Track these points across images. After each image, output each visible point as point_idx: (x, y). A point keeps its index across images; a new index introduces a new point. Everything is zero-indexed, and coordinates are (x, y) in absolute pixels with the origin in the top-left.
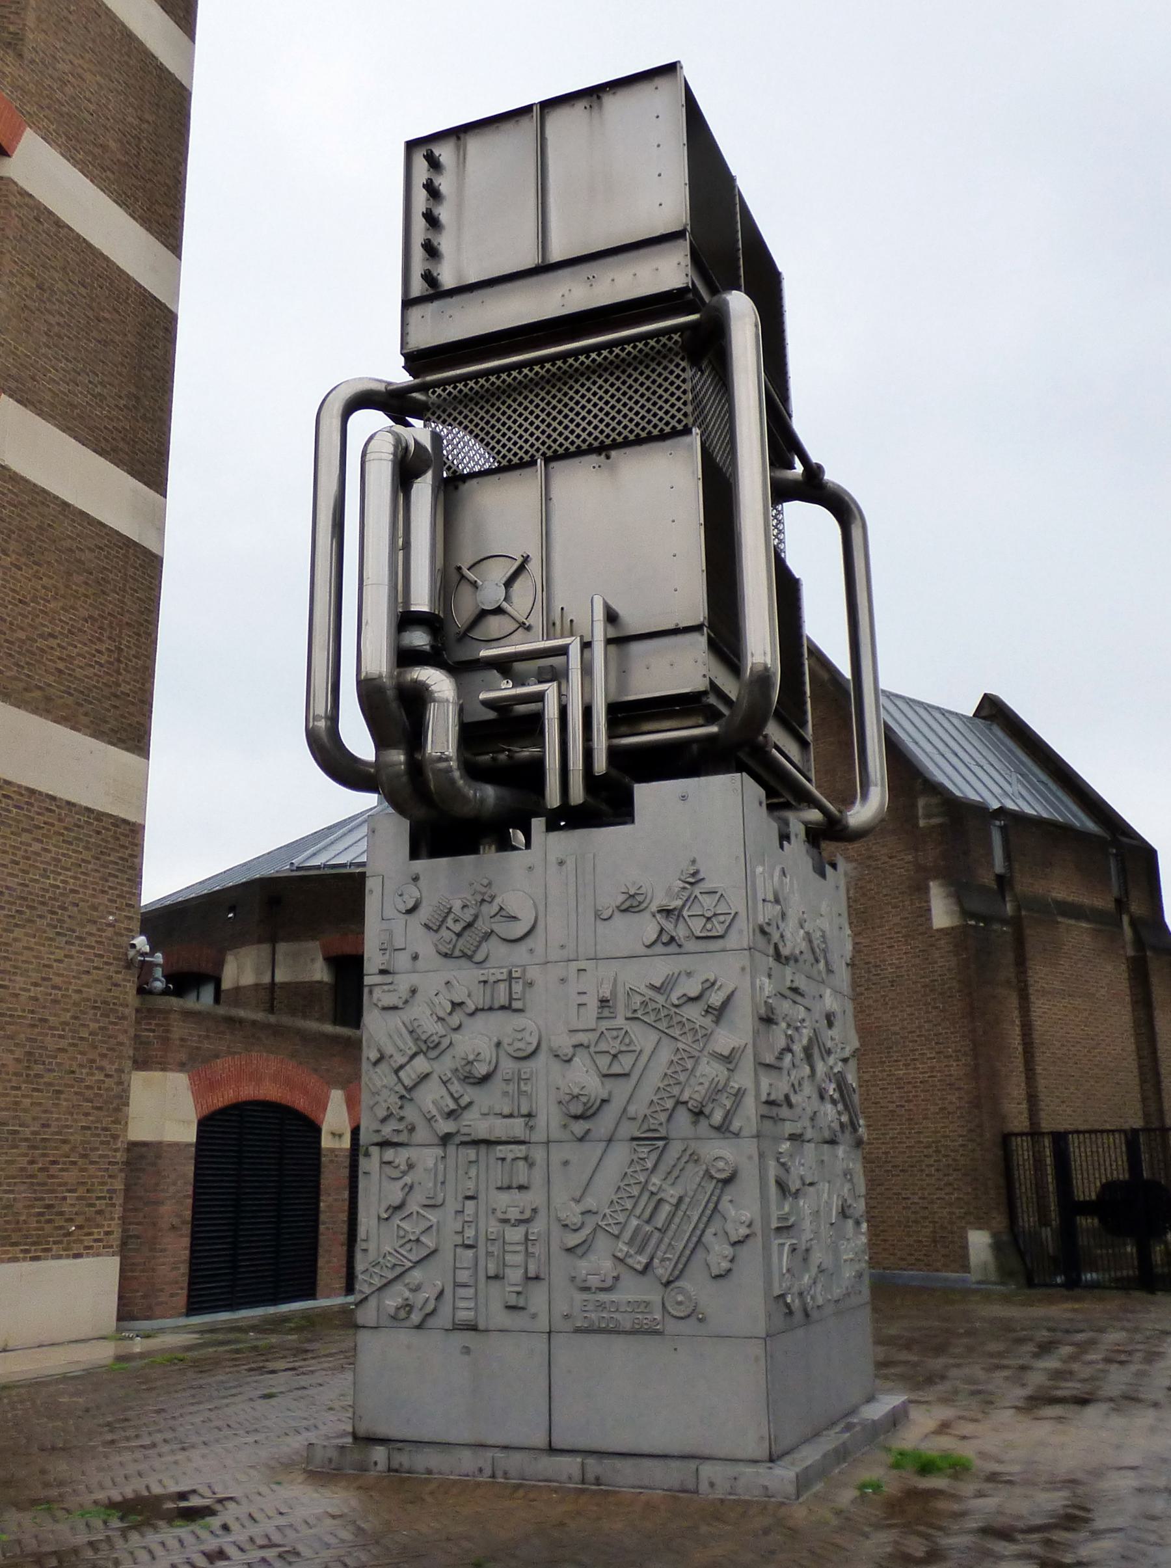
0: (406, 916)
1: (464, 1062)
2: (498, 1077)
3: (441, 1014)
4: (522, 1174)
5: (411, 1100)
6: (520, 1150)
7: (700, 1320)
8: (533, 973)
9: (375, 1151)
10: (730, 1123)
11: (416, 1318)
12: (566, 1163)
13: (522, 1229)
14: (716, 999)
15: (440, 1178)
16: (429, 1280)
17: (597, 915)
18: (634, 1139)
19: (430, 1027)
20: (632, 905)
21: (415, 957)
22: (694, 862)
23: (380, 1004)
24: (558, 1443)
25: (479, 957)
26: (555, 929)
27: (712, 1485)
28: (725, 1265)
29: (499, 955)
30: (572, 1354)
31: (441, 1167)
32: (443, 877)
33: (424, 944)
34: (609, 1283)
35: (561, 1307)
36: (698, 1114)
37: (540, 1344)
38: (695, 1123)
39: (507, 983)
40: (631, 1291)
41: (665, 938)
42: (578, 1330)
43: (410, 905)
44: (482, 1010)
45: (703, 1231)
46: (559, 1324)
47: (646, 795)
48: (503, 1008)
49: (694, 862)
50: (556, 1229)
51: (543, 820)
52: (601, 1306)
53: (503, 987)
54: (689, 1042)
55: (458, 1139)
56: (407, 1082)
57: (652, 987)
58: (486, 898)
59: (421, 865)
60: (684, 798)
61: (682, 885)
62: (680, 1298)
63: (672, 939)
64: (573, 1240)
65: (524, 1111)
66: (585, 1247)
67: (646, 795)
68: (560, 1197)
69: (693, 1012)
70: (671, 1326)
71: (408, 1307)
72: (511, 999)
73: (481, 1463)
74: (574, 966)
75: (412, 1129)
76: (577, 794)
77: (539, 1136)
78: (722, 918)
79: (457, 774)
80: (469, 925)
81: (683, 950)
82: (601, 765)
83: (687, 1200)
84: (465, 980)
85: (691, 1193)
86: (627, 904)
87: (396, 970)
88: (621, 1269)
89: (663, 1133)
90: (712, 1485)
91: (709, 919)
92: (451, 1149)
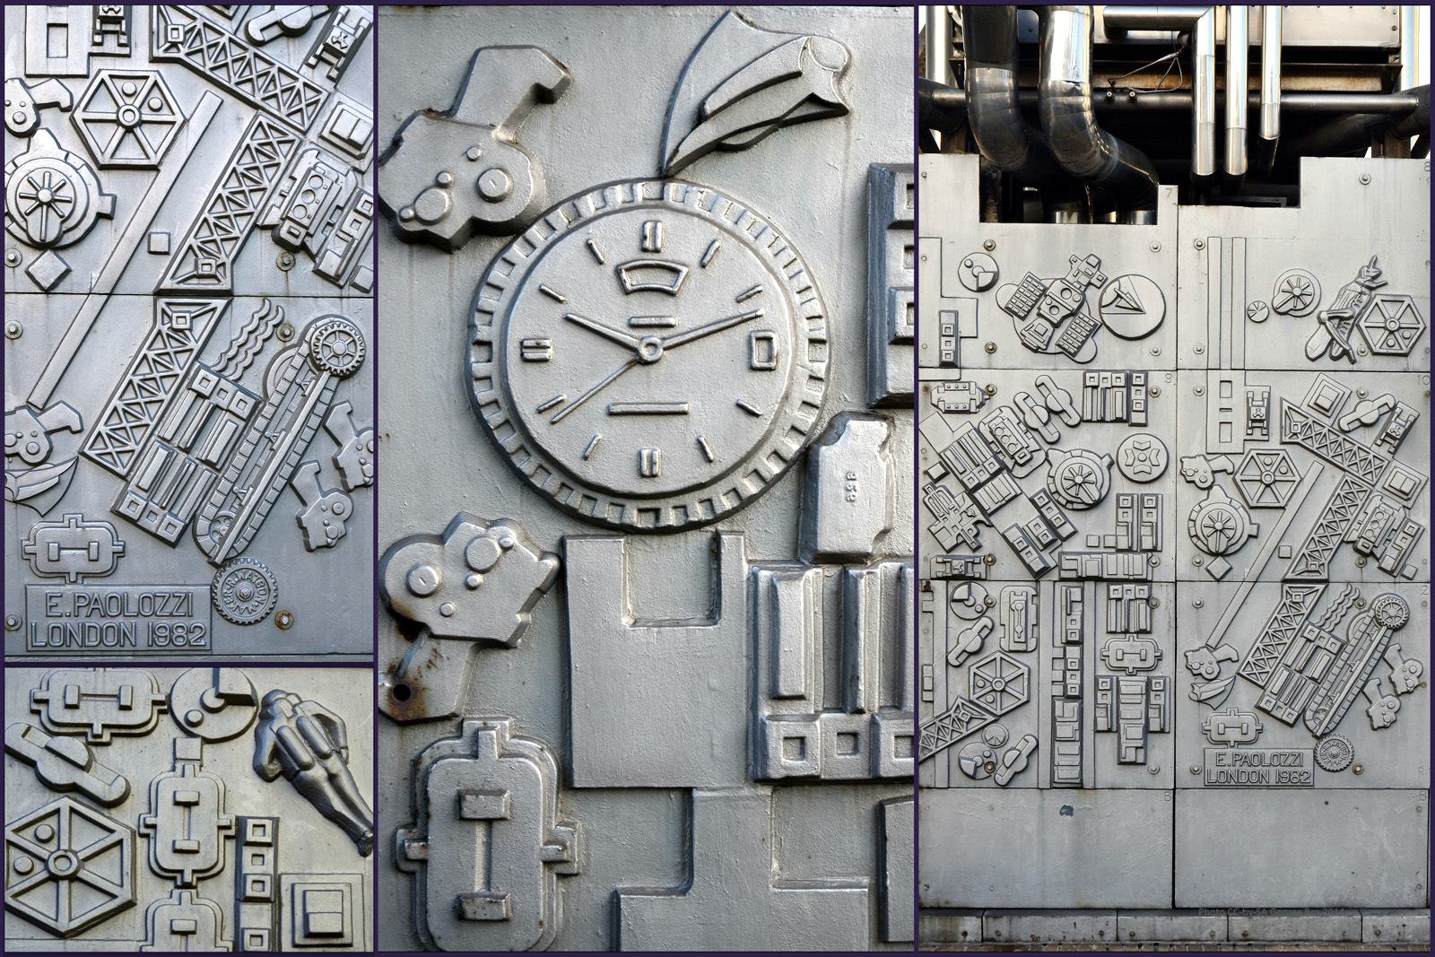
0: (979, 295)
1: (1207, 521)
2: (1111, 503)
3: (1033, 423)
4: (1140, 616)
5: (991, 526)
6: (1142, 591)
7: (1355, 772)
8: (1156, 380)
9: (939, 586)
10: (1404, 566)
11: (1003, 776)
12: (1199, 606)
13: (1142, 677)
14: (1396, 428)
15: (1032, 620)
16: (1022, 731)
17: (1248, 315)
18: (1285, 581)
19: (1015, 439)
20: (1295, 305)
21: (991, 350)
22: (1374, 262)
23: (941, 405)
24: (1184, 900)
25: (1084, 355)
26: (1191, 325)
27: (1378, 933)
28: (1390, 716)
29: (1111, 355)
30: (1201, 813)
31: (1032, 608)
32: (1043, 248)
33: (1002, 330)
34: (1251, 736)
35: (1187, 761)
36: (1366, 555)
37: (1162, 803)
38: (1362, 565)
39: (1124, 390)
40: (1276, 740)
41: (1336, 351)
42: (1210, 786)
43: (985, 280)
44: (1090, 421)
45: (1366, 682)
46: (1185, 779)
47: (1311, 167)
48: (1118, 420)
49: (1374, 262)
50: (1185, 679)
51: (1175, 188)
52: (1245, 759)
53: (1120, 395)
54: (1360, 475)
55: (1054, 575)
56: (989, 505)
57: (1319, 408)
58: (1094, 281)
59: (998, 230)
60: (1365, 181)
61: (1359, 289)
62: (245, 588)
63: (1345, 353)
64: (1207, 690)
65: (1147, 544)
66: (1225, 695)
67: (1311, 167)
68: (1188, 641)
69: (1366, 438)
70: (1322, 779)
71: (991, 766)
72: (1129, 410)
73: (1101, 926)
74: (1215, 377)
75: (991, 561)
76: (1237, 162)
77: (1163, 573)
78: (1407, 334)
79: (1088, 115)
80: (1073, 314)
81: (1355, 367)
82: (1270, 128)
83: (1349, 649)
84: (1066, 377)
85: (1353, 642)
86: (1290, 305)
87: (963, 364)
88: (1264, 718)
89: (1324, 576)
90: (1378, 933)
91: (1392, 332)
92: (1045, 585)
